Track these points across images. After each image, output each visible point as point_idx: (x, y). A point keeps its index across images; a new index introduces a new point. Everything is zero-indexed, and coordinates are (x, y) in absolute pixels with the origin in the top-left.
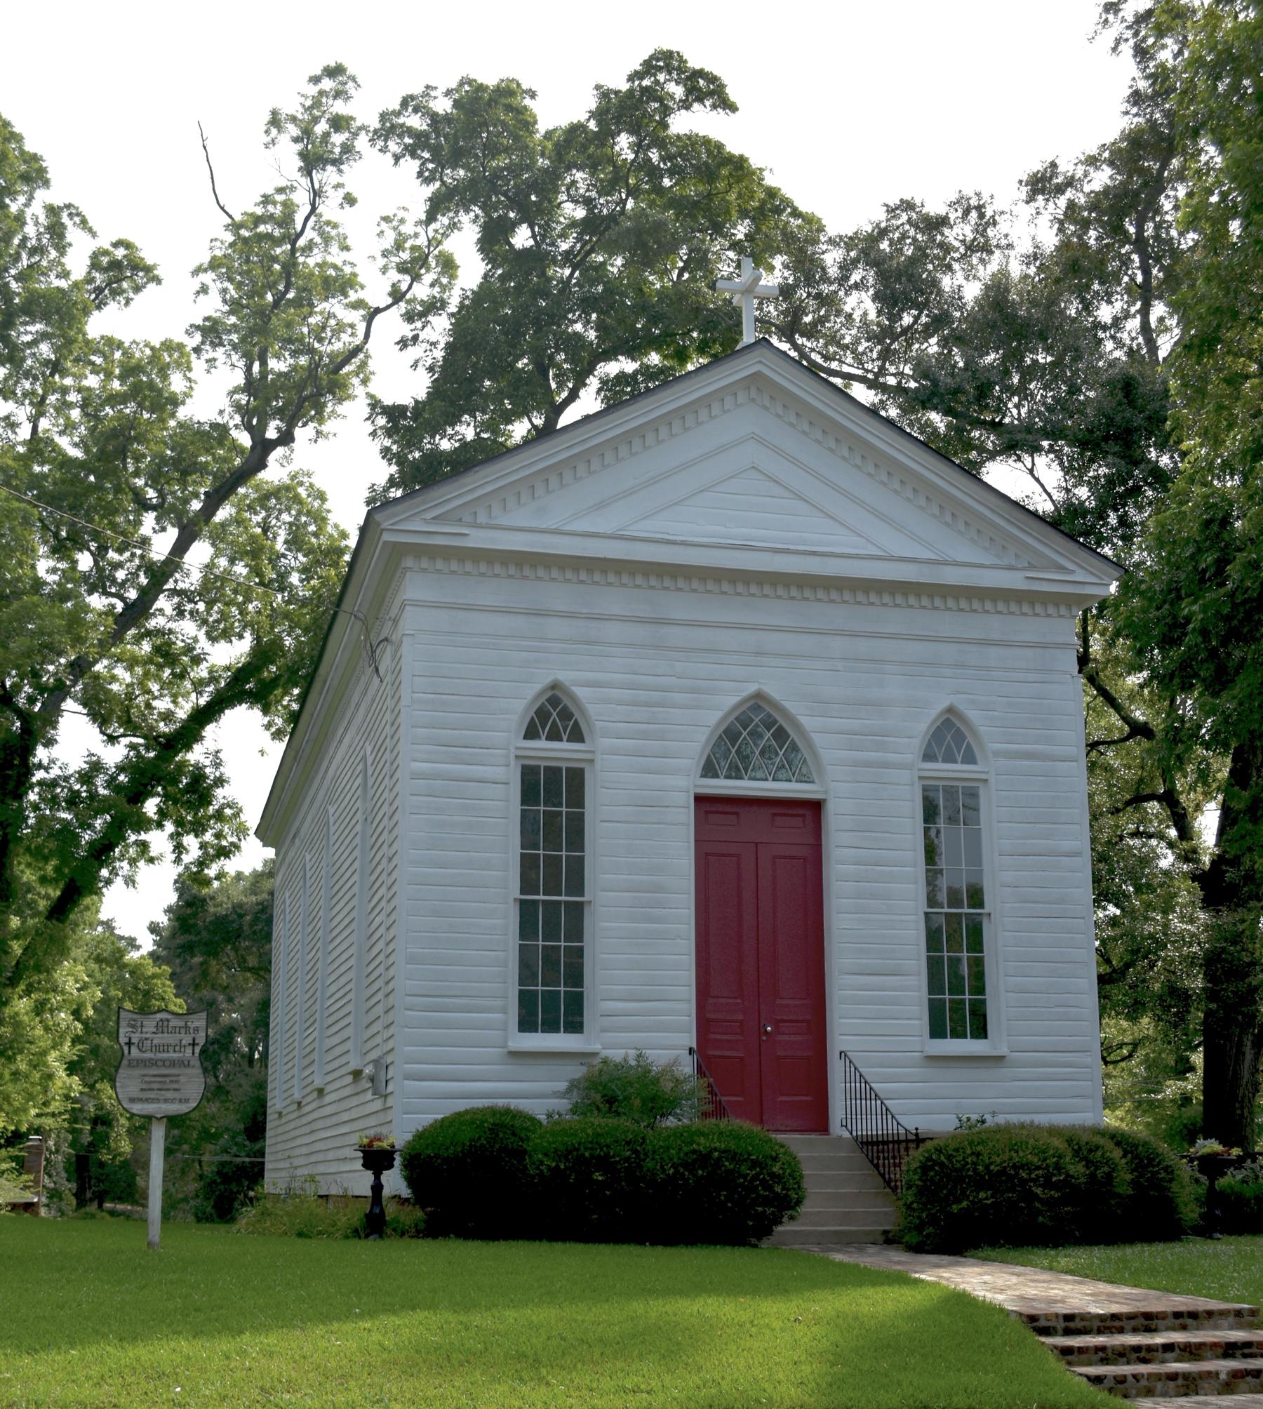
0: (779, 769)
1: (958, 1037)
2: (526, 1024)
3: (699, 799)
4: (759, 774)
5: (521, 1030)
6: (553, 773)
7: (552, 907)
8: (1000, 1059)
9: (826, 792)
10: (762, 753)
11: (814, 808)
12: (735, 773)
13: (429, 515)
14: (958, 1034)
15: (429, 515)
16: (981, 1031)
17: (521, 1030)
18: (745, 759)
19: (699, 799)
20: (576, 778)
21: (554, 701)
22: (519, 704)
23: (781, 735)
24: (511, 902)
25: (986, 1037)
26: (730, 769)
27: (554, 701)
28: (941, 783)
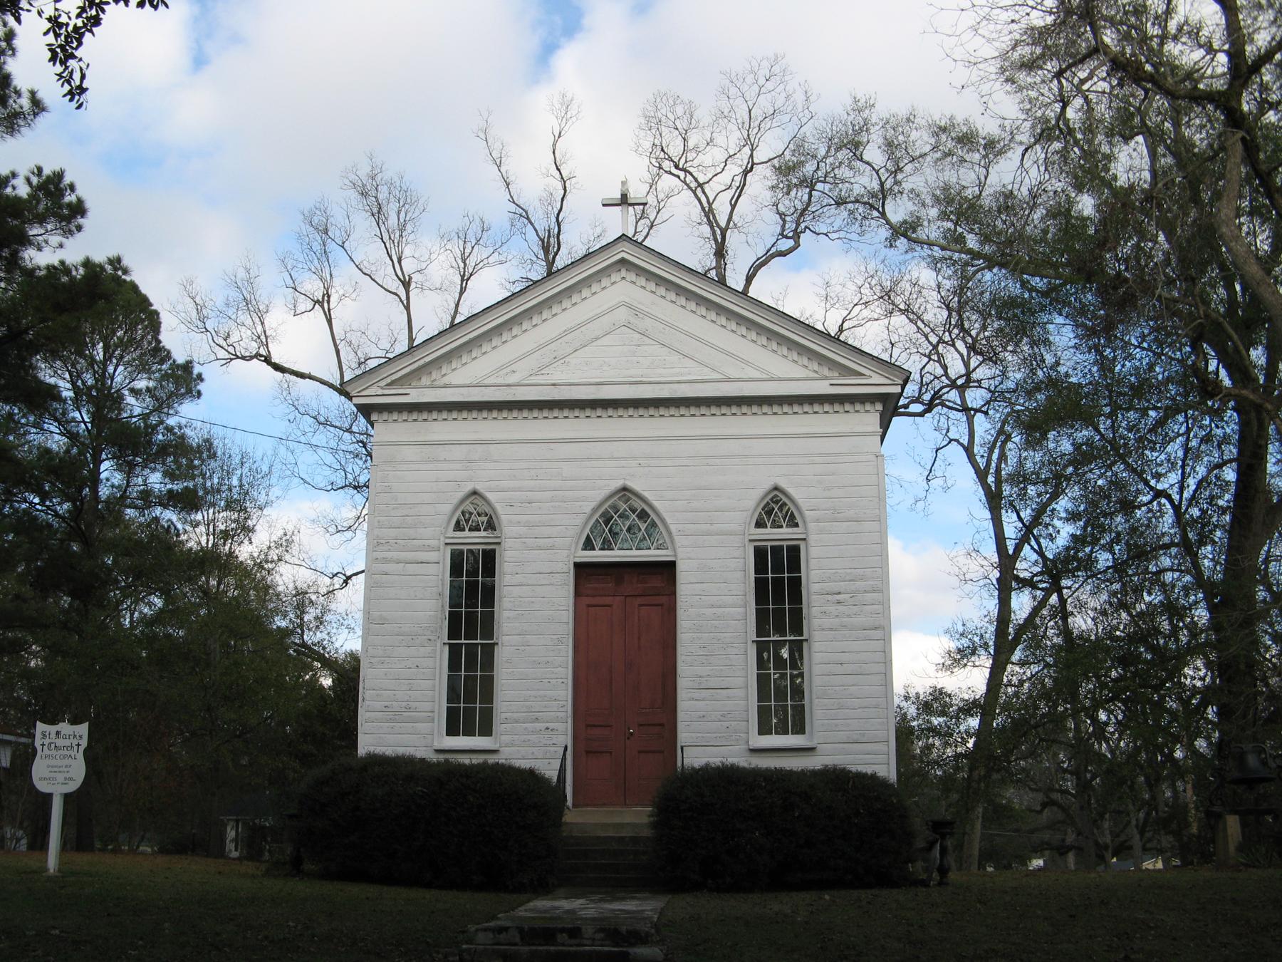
0: (641, 541)
1: (797, 733)
2: (764, 729)
3: (579, 567)
4: (626, 546)
5: (448, 734)
6: (777, 550)
7: (471, 649)
8: (812, 749)
9: (675, 556)
10: (629, 530)
11: (669, 568)
12: (607, 546)
13: (383, 383)
14: (469, 732)
15: (383, 383)
16: (487, 730)
17: (448, 734)
18: (615, 535)
19: (579, 567)
20: (794, 552)
21: (775, 500)
22: (751, 500)
23: (643, 515)
24: (749, 642)
25: (804, 733)
26: (604, 542)
27: (775, 500)
28: (785, 544)
